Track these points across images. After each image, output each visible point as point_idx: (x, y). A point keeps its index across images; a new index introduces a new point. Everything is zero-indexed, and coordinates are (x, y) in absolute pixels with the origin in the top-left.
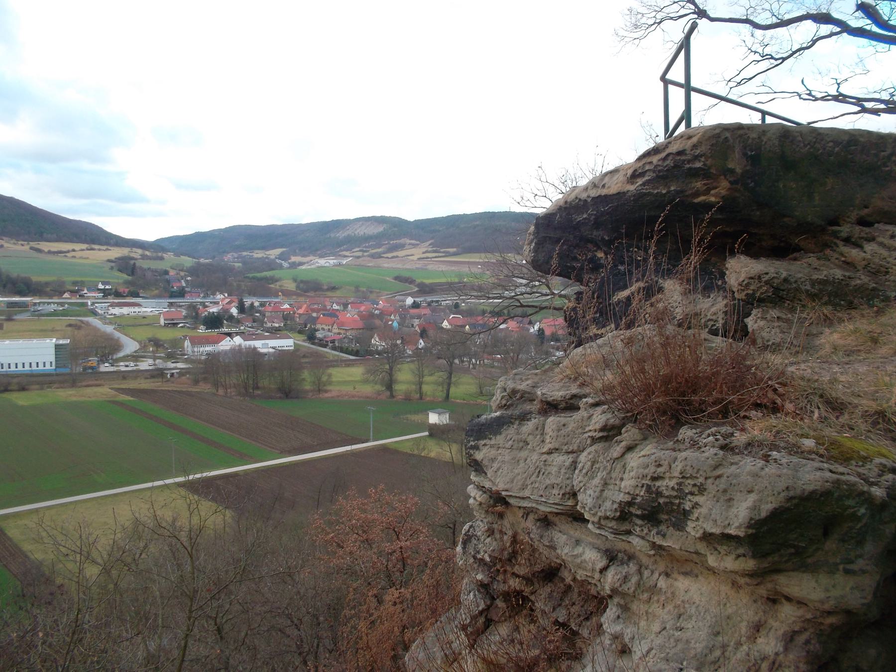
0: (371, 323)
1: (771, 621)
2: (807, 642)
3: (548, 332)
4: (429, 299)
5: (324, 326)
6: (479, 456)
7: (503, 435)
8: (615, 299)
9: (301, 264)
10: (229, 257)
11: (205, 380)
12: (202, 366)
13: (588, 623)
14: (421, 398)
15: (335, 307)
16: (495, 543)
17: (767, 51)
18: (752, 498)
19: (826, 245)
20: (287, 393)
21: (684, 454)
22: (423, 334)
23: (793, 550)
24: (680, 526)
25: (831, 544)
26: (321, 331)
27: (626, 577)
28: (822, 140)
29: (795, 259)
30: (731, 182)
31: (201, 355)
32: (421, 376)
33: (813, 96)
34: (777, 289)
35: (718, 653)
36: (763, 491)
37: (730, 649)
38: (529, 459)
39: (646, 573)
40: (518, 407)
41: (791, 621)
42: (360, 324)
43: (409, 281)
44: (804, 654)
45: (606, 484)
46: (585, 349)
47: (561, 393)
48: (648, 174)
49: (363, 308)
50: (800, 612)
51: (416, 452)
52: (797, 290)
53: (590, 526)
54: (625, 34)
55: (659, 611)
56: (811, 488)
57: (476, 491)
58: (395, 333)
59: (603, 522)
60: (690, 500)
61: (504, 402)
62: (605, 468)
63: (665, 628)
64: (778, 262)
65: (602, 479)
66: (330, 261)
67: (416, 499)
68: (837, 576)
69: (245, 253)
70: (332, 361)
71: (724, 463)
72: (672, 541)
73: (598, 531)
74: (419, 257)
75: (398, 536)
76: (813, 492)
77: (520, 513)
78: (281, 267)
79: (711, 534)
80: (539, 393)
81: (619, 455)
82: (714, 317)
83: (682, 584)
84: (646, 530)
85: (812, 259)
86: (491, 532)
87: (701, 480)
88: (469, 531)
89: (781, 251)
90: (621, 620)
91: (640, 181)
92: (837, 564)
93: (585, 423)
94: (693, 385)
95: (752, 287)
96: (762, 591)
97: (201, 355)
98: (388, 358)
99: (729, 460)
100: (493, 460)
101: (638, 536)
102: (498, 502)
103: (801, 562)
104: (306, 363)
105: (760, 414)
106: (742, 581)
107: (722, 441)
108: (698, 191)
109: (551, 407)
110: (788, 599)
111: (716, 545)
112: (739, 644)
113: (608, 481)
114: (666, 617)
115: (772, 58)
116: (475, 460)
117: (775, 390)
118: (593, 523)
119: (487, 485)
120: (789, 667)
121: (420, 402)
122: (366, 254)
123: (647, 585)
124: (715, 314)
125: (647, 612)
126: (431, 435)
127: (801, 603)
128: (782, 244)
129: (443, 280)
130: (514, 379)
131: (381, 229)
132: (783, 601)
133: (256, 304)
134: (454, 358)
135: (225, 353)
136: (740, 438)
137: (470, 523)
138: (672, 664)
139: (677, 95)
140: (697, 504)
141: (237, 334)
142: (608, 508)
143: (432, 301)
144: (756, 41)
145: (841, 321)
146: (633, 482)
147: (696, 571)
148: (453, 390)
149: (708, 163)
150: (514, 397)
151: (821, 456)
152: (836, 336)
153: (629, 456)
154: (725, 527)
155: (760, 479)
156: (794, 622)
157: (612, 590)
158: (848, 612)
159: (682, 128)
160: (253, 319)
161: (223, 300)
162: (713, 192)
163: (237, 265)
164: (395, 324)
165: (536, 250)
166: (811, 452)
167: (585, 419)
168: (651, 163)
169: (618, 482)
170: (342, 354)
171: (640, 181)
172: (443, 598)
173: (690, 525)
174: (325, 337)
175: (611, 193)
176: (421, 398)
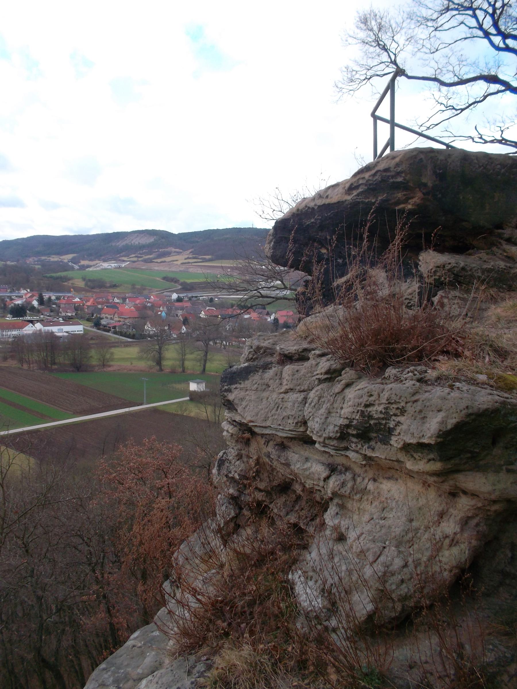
0: (144, 313)
1: (451, 510)
2: (477, 525)
3: (281, 321)
4: (190, 295)
5: (107, 315)
6: (231, 397)
7: (250, 380)
8: (335, 284)
9: (89, 266)
10: (30, 261)
11: (13, 357)
12: (9, 346)
13: (314, 523)
14: (184, 371)
15: (116, 300)
16: (242, 465)
17: (450, 103)
18: (440, 416)
19: (493, 244)
20: (78, 367)
21: (390, 386)
22: (185, 322)
23: (469, 455)
24: (385, 441)
25: (497, 451)
26: (105, 320)
27: (343, 483)
28: (492, 163)
29: (470, 255)
30: (424, 194)
31: (9, 338)
32: (184, 354)
33: (483, 140)
34: (456, 276)
35: (410, 535)
36: (449, 409)
37: (420, 531)
38: (270, 398)
39: (359, 480)
40: (261, 360)
41: (466, 509)
42: (136, 314)
43: (174, 280)
44: (475, 533)
45: (329, 412)
46: (312, 318)
47: (295, 348)
48: (361, 187)
49: (138, 302)
50: (473, 502)
51: (180, 413)
52: (472, 276)
53: (317, 445)
54: (343, 86)
55: (368, 507)
56: (485, 407)
57: (228, 425)
58: (163, 321)
59: (327, 442)
60: (394, 420)
61: (251, 356)
62: (329, 401)
63: (373, 518)
64: (458, 256)
65: (326, 409)
66: (113, 265)
67: (180, 447)
68: (501, 474)
69: (43, 258)
70: (113, 343)
71: (420, 391)
72: (380, 453)
73: (323, 449)
74: (182, 262)
75: (166, 475)
76: (487, 410)
77: (262, 441)
78: (73, 268)
79: (409, 444)
80: (278, 348)
81: (340, 390)
82: (410, 297)
83: (386, 486)
84: (359, 446)
85: (483, 255)
86: (239, 457)
87: (403, 404)
88: (223, 456)
89: (460, 248)
90: (339, 516)
91: (355, 193)
92: (501, 466)
93: (313, 369)
94: (397, 336)
95: (438, 274)
96: (446, 487)
97: (9, 338)
98: (158, 340)
99: (423, 389)
100: (242, 399)
101: (353, 451)
102: (247, 433)
103: (475, 464)
104: (93, 344)
105: (446, 358)
106: (431, 480)
107: (418, 376)
108: (399, 200)
109: (287, 358)
110: (465, 493)
111: (413, 453)
112: (427, 528)
113: (331, 411)
114: (373, 510)
115: (454, 108)
116: (229, 401)
117: (457, 341)
118: (319, 443)
119: (238, 418)
120: (464, 543)
121: (183, 375)
122: (140, 259)
123: (360, 489)
124: (410, 294)
125: (359, 509)
126: (191, 400)
127: (474, 495)
128: (460, 244)
129: (201, 280)
130: (258, 339)
131: (152, 240)
132: (461, 494)
133: (53, 298)
134: (210, 340)
135: (29, 336)
136: (431, 374)
137: (224, 451)
138: (377, 544)
139: (384, 129)
140: (399, 422)
141: (38, 321)
142: (331, 430)
143: (193, 297)
144: (442, 95)
145: (503, 299)
146: (350, 409)
147: (396, 476)
148: (208, 365)
149: (407, 178)
150: (258, 352)
151: (491, 386)
152: (499, 310)
153: (347, 391)
154: (420, 438)
155: (447, 401)
156: (469, 509)
157: (333, 494)
158: (509, 501)
159: (388, 151)
160: (50, 310)
161: (26, 294)
162: (410, 201)
163: (37, 267)
164: (164, 314)
165: (274, 248)
166: (483, 383)
167: (313, 366)
168: (363, 178)
169: (339, 411)
170: (121, 337)
171: (355, 193)
172: (201, 512)
173: (393, 440)
174: (108, 324)
175: (332, 202)
176: (184, 371)
